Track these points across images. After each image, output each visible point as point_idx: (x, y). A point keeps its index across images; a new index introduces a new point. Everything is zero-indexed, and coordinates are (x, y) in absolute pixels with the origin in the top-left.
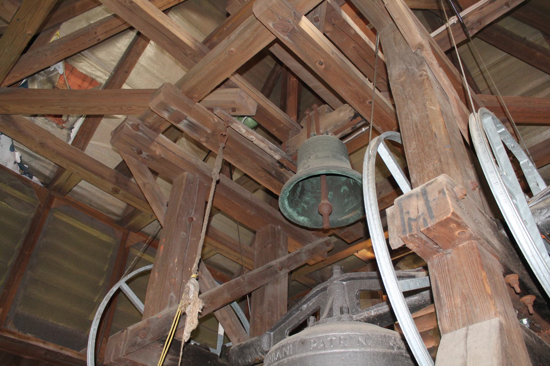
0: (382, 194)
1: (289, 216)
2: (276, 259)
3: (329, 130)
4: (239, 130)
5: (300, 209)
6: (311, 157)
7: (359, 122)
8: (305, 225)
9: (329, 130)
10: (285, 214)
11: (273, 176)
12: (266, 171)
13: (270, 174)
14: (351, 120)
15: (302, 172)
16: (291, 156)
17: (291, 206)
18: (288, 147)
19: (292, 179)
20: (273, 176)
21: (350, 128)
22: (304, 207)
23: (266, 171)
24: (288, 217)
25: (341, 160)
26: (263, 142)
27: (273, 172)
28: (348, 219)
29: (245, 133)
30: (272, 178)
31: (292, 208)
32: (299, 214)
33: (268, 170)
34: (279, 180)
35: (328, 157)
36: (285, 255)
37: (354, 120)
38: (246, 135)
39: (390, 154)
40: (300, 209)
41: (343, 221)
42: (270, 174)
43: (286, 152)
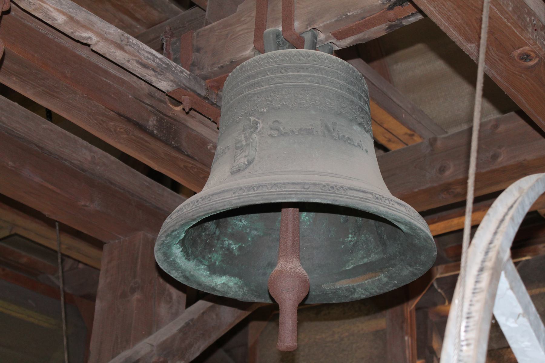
0: (448, 173)
1: (185, 277)
2: (150, 334)
3: (319, 25)
4: (47, 15)
5: (217, 257)
6: (260, 126)
7: (409, 17)
8: (230, 295)
9: (319, 25)
10: (174, 274)
11: (151, 134)
12: (129, 120)
13: (142, 128)
14: (391, 8)
15: (222, 187)
16: (205, 78)
17: (188, 255)
18: (198, 50)
19: (190, 208)
20: (151, 134)
21: (384, 26)
22: (229, 249)
23: (129, 120)
24: (181, 280)
25: (348, 141)
26: (120, 47)
27: (152, 123)
28: (352, 290)
29: (66, 23)
30: (147, 138)
31: (196, 257)
32: (213, 270)
33: (135, 118)
34: (166, 143)
35: (310, 132)
36: (175, 315)
37: (397, 8)
38: (68, 30)
39: (526, 313)
40: (217, 257)
41: (335, 292)
42: (142, 128)
43: (192, 66)
